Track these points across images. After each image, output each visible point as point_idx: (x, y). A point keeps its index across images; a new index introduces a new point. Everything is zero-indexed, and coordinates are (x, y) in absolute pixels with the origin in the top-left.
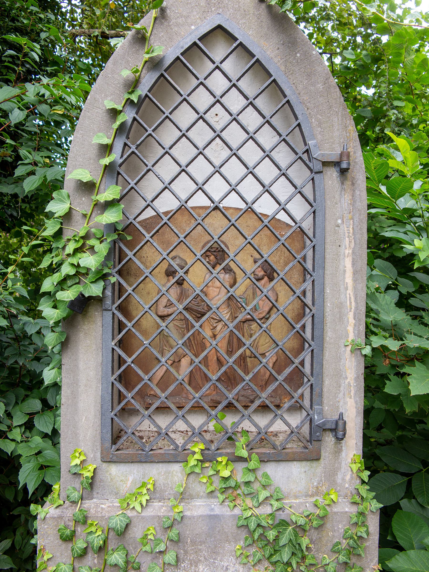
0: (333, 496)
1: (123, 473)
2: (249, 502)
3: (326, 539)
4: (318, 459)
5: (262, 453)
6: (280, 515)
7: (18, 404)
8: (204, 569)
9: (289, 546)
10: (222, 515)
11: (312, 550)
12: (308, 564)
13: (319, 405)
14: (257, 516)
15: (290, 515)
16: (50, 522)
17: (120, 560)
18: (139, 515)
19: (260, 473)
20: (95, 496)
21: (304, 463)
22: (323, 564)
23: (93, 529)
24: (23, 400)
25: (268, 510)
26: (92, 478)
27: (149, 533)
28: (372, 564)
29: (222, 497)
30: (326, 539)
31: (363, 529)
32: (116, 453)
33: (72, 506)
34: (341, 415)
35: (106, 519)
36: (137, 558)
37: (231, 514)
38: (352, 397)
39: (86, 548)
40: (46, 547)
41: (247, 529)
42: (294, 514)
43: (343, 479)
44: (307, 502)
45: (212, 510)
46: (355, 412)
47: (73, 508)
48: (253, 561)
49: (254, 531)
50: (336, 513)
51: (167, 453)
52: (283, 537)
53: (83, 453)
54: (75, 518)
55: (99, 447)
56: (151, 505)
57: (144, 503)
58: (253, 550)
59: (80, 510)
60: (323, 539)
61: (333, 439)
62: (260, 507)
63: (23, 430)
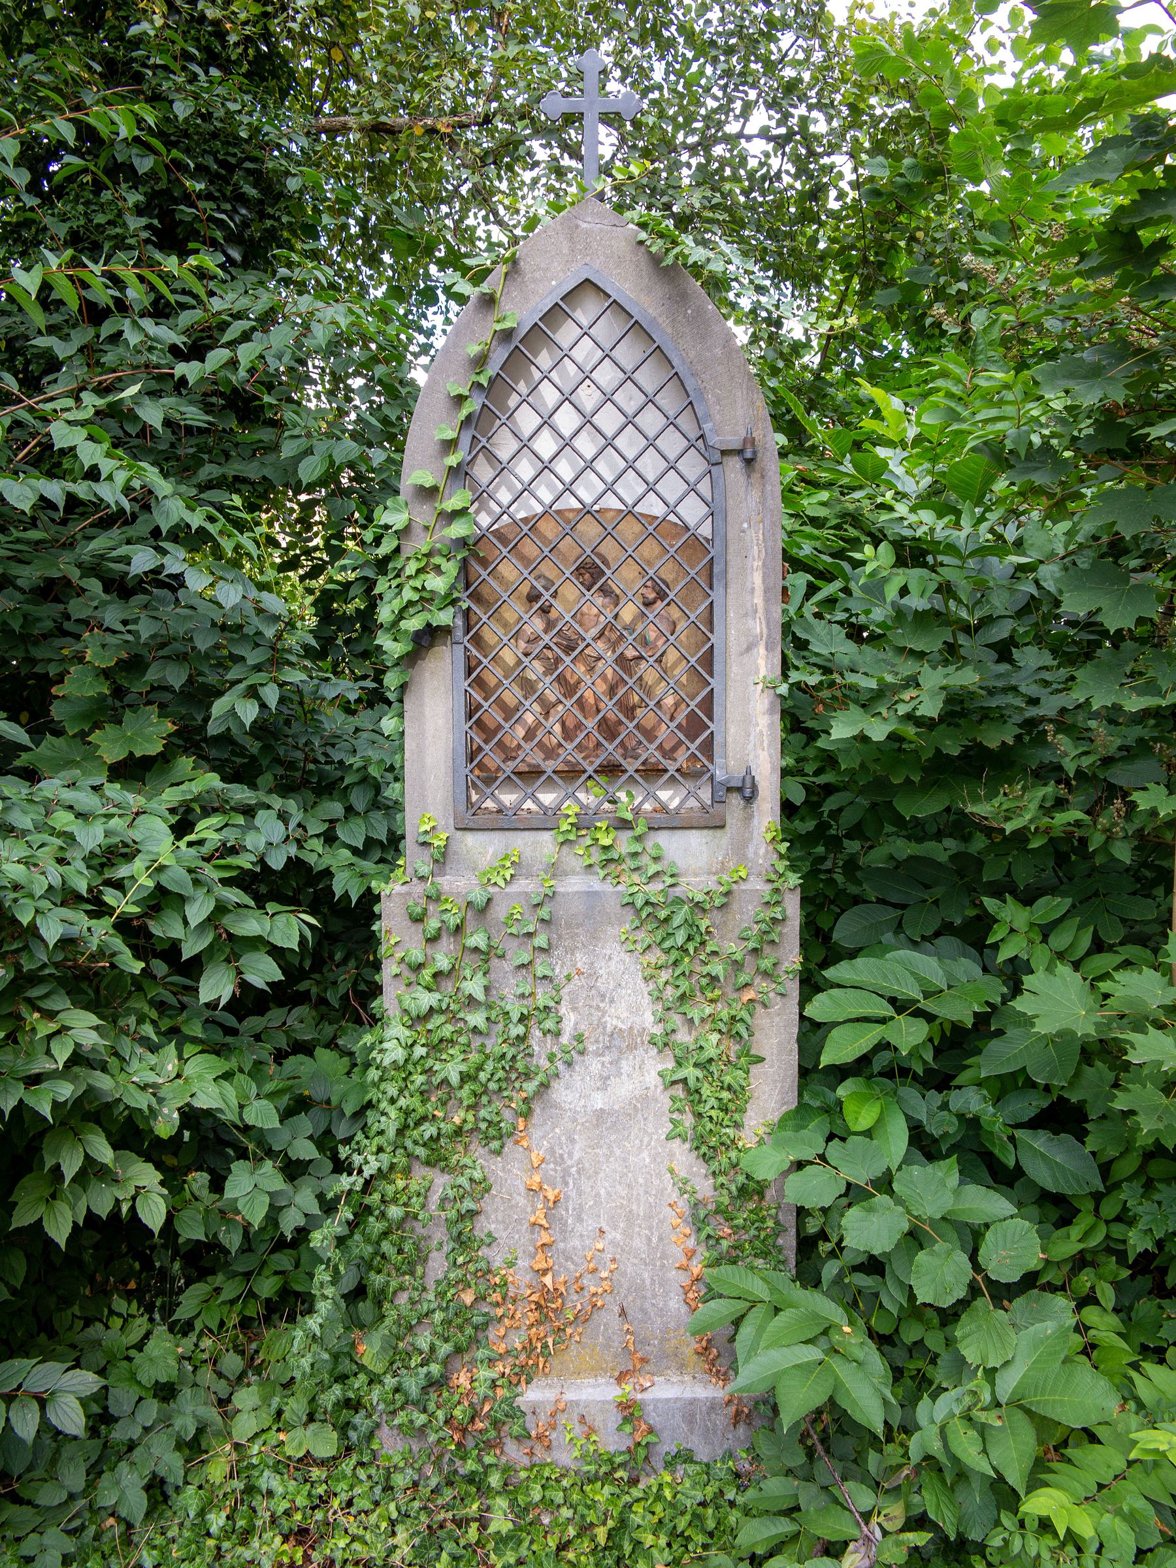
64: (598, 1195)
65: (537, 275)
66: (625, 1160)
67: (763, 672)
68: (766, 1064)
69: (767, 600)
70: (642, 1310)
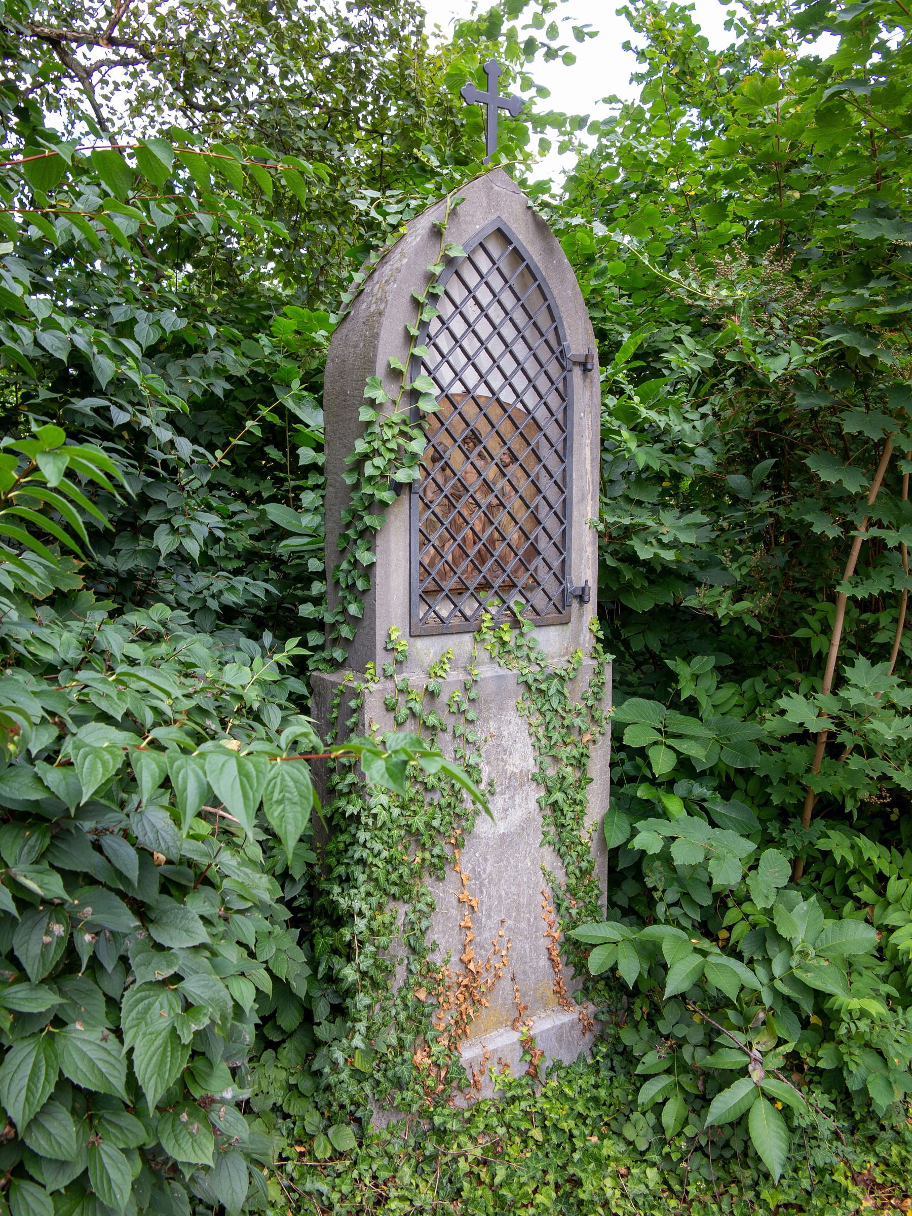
64: (500, 896)
65: (468, 219)
66: (516, 867)
67: (590, 516)
68: (593, 784)
69: (592, 467)
70: (524, 972)
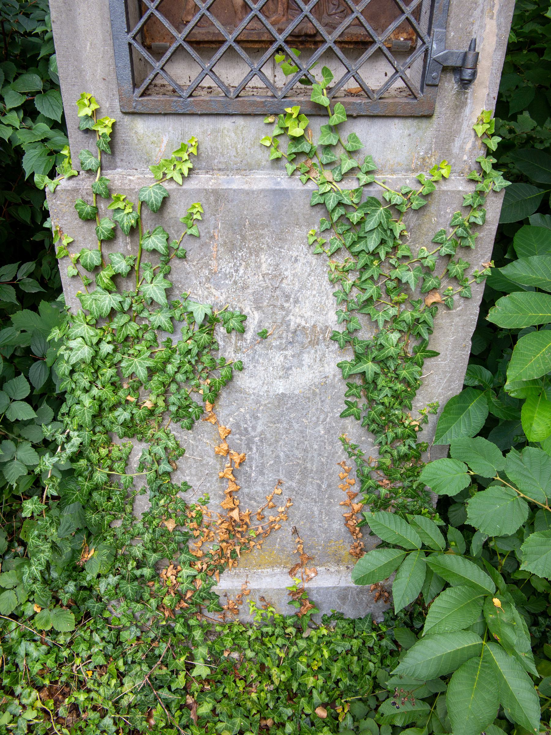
0: (445, 172)
1: (153, 131)
2: (328, 175)
3: (427, 226)
4: (429, 117)
5: (349, 104)
6: (370, 192)
7: (10, 83)
8: (267, 259)
9: (378, 232)
10: (291, 190)
11: (408, 240)
12: (400, 256)
13: (441, 27)
14: (337, 192)
15: (382, 193)
16: (63, 197)
17: (159, 245)
18: (179, 187)
19: (345, 135)
20: (119, 164)
21: (409, 122)
22: (420, 257)
23: (121, 205)
24: (15, 78)
25: (354, 185)
26: (112, 135)
27: (194, 211)
28: (482, 261)
29: (291, 168)
30: (427, 226)
31: (478, 214)
32: (140, 99)
33: (89, 178)
34: (473, 44)
35: (136, 192)
36: (181, 244)
37: (303, 188)
38: (495, 17)
39: (114, 230)
40: (63, 229)
41: (324, 210)
42: (388, 191)
43: (462, 148)
44: (408, 178)
45: (278, 183)
46: (494, 43)
47: (91, 179)
48: (330, 251)
49: (333, 210)
50: (444, 192)
51: (214, 101)
52: (370, 221)
53: (93, 100)
54: (94, 190)
55: (116, 92)
56: (196, 177)
57: (186, 174)
58: (330, 237)
59: (100, 180)
60: (423, 226)
61: (456, 86)
62: (343, 182)
63: (22, 116)
68: (439, 359)
